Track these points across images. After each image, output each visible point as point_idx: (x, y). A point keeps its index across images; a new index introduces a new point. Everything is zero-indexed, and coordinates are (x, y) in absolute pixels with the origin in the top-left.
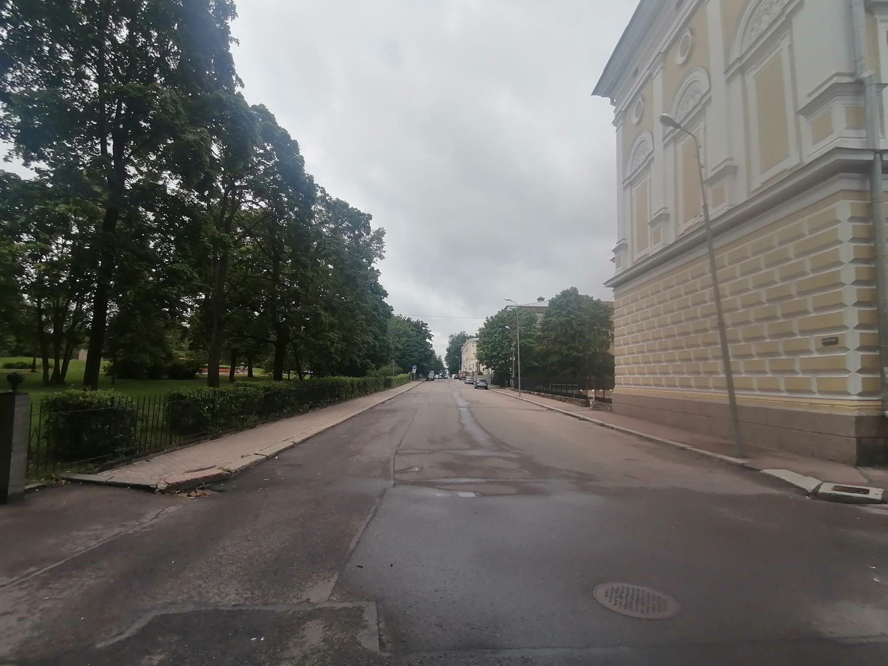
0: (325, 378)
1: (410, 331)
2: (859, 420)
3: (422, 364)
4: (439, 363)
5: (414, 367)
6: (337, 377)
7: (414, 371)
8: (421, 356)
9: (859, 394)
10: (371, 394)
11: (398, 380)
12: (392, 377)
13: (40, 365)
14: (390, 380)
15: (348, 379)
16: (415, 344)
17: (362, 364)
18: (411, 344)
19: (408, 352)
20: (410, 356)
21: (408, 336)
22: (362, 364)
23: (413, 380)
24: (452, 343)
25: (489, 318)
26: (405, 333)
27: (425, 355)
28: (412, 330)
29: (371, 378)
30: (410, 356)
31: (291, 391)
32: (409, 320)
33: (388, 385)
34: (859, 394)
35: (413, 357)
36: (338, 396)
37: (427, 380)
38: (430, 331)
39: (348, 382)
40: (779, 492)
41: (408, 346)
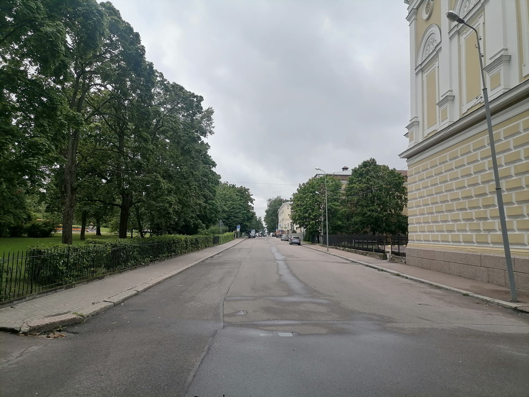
0: (163, 236)
3: (244, 223)
6: (173, 235)
8: (244, 217)
15: (183, 237)
17: (194, 224)
19: (233, 213)
20: (235, 217)
22: (194, 224)
23: (237, 238)
26: (230, 197)
29: (202, 236)
30: (235, 217)
33: (216, 241)
35: (238, 218)
36: (174, 251)
37: (249, 237)
38: (252, 195)
39: (183, 239)
41: (233, 208)
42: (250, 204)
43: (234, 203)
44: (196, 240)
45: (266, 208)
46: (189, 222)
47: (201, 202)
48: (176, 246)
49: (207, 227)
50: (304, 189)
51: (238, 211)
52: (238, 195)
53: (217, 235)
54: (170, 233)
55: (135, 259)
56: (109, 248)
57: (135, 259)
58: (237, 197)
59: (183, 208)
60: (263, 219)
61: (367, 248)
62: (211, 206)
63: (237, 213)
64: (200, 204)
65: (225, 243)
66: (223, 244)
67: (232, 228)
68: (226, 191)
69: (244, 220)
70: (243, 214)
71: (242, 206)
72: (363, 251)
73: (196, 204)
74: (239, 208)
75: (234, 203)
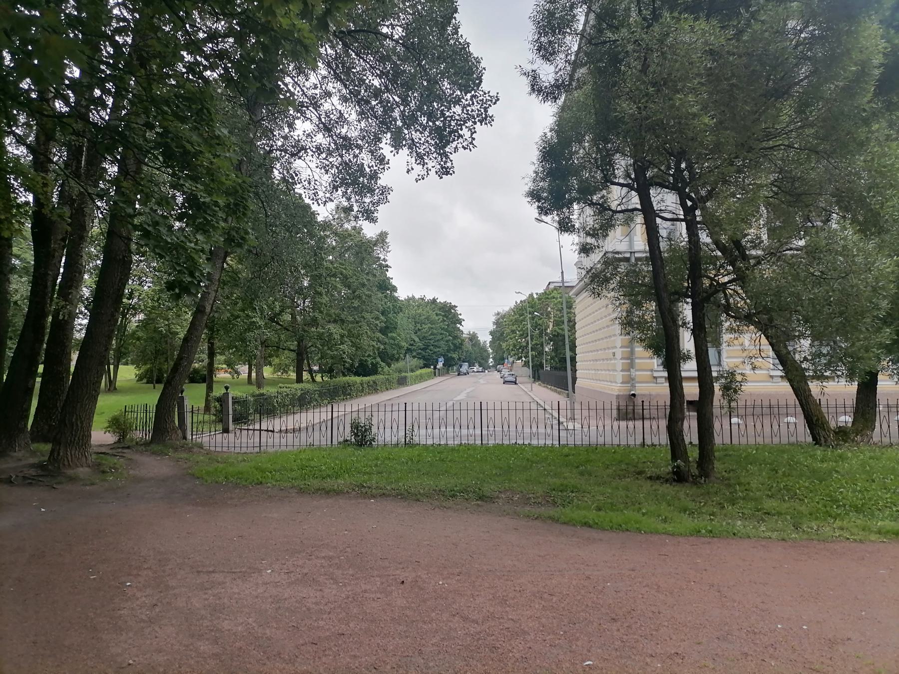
0: (338, 379)
1: (435, 316)
2: (618, 397)
3: (450, 355)
4: (483, 349)
5: (440, 360)
6: (348, 378)
7: (440, 365)
8: (449, 346)
9: (622, 383)
10: (382, 392)
11: (417, 377)
12: (406, 374)
13: (193, 381)
14: (405, 377)
15: (358, 379)
16: (440, 331)
17: (372, 363)
18: (435, 331)
19: (432, 342)
20: (435, 346)
21: (432, 323)
22: (372, 363)
23: (439, 376)
24: (497, 323)
25: (519, 302)
26: (428, 318)
27: (455, 345)
28: (437, 315)
29: (382, 377)
30: (435, 346)
31: (316, 390)
32: (434, 301)
33: (402, 382)
34: (622, 383)
35: (439, 347)
36: (349, 394)
37: (459, 375)
38: (460, 314)
39: (358, 382)
40: (49, 324)
41: (432, 334)
42: (458, 325)
43: (433, 326)
44: (374, 382)
45: (492, 327)
46: (366, 361)
47: (374, 343)
48: (351, 389)
49: (389, 365)
50: (521, 309)
51: (439, 337)
52: (440, 314)
53: (403, 374)
54: (344, 375)
55: (316, 400)
56: (299, 391)
57: (316, 400)
58: (437, 318)
59: (357, 350)
60: (488, 342)
61: (805, 379)
62: (392, 342)
63: (438, 340)
64: (373, 346)
65: (415, 383)
66: (412, 385)
67: (428, 362)
68: (420, 310)
69: (448, 351)
70: (447, 341)
71: (446, 330)
72: (368, 378)
73: (369, 346)
74: (441, 334)
75: (433, 326)
